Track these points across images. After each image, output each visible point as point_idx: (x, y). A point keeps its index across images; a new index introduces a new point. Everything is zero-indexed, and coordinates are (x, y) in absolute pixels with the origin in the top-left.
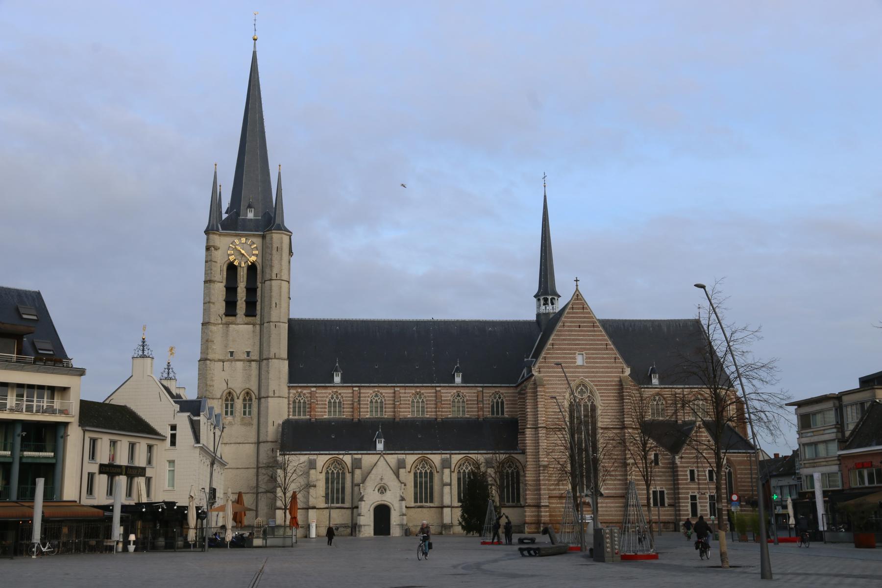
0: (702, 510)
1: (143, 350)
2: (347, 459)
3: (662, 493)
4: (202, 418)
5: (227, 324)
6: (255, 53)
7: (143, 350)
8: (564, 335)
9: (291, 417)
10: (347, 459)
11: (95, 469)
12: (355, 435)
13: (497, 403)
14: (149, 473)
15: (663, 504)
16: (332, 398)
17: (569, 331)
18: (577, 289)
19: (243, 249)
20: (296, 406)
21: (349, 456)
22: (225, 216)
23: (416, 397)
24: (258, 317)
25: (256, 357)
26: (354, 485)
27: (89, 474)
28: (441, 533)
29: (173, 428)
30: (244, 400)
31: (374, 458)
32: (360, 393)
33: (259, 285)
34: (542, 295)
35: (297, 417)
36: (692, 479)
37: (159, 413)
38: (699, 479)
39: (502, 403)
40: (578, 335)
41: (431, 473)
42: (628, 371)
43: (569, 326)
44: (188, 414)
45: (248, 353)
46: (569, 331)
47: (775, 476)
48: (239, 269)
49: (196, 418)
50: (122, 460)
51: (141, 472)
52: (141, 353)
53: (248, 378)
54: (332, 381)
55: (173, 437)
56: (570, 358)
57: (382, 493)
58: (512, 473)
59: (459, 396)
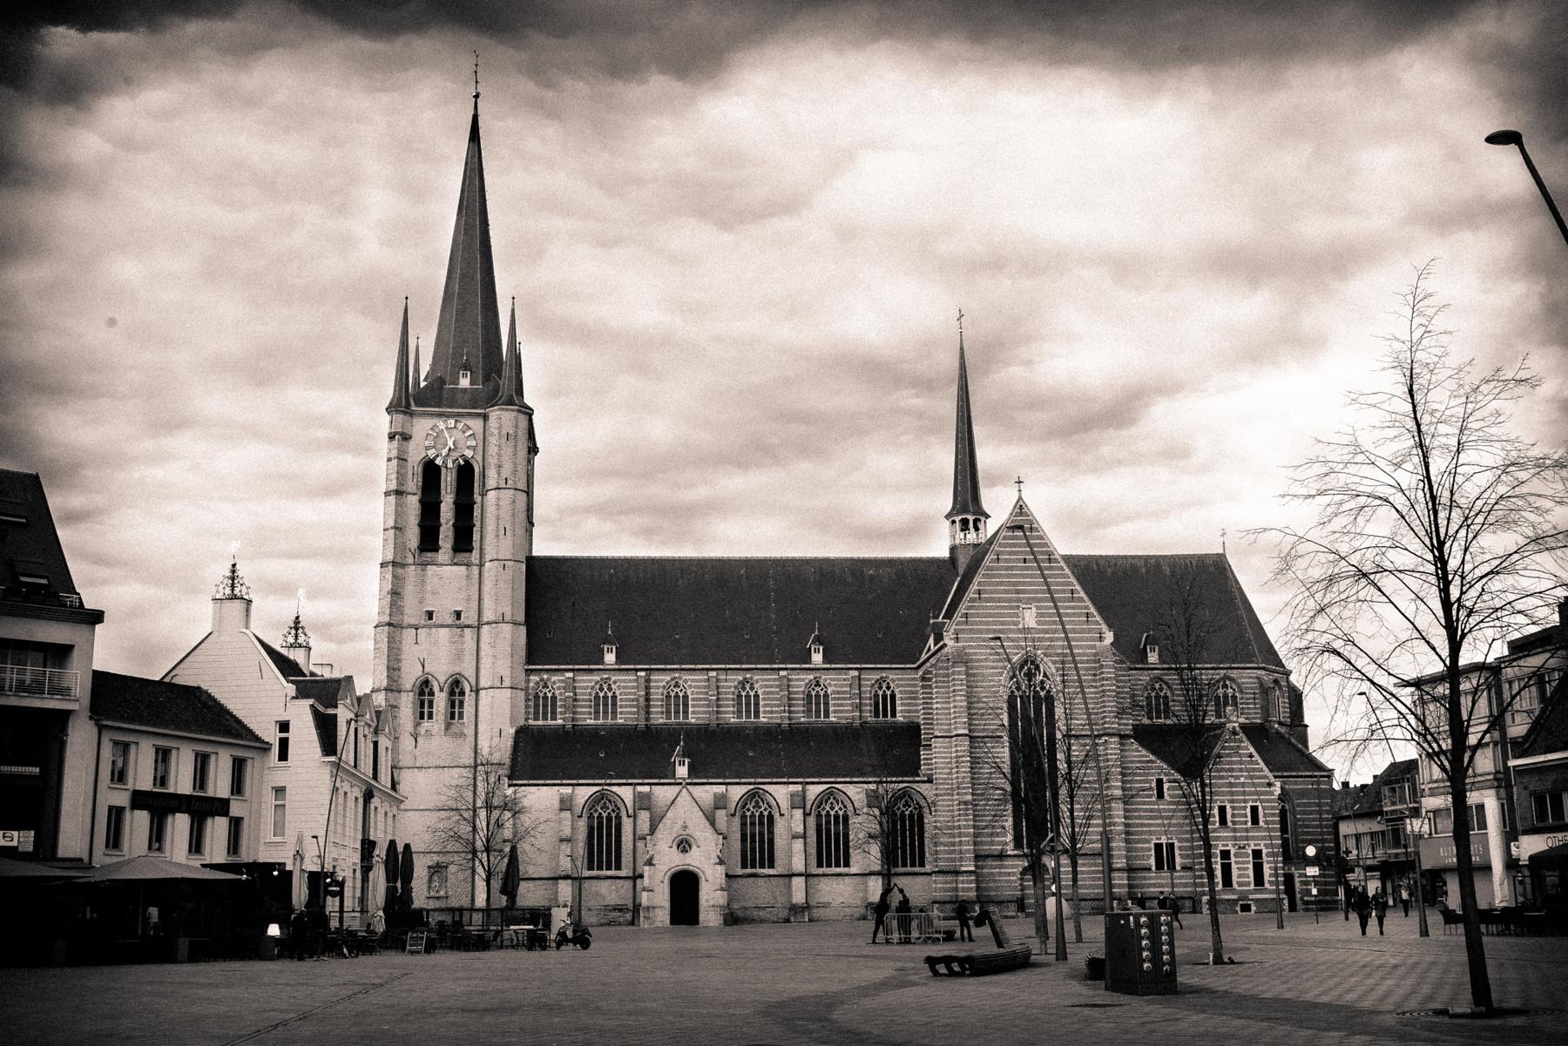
0: (1239, 876)
1: (233, 586)
2: (626, 793)
3: (1171, 846)
4: (343, 713)
5: (425, 564)
6: (475, 118)
7: (233, 586)
8: (1000, 576)
9: (531, 722)
10: (626, 793)
11: (122, 799)
12: (642, 750)
13: (885, 697)
14: (236, 809)
15: (1172, 867)
16: (601, 689)
17: (1007, 568)
18: (1020, 498)
19: (445, 437)
20: (540, 703)
21: (629, 789)
22: (423, 384)
23: (744, 688)
24: (476, 553)
25: (473, 621)
26: (637, 838)
27: (111, 808)
28: (788, 921)
29: (284, 727)
30: (452, 693)
31: (670, 792)
32: (648, 681)
33: (477, 498)
34: (958, 514)
35: (540, 722)
36: (1255, 820)
37: (262, 701)
38: (1234, 823)
39: (893, 697)
40: (1023, 576)
41: (771, 817)
42: (1109, 637)
43: (1007, 561)
44: (311, 701)
45: (458, 614)
46: (1007, 568)
47: (1348, 818)
48: (443, 470)
49: (331, 711)
50: (182, 782)
51: (220, 807)
52: (228, 591)
53: (459, 656)
54: (601, 660)
55: (284, 743)
56: (1010, 615)
57: (684, 851)
58: (911, 815)
59: (818, 685)
